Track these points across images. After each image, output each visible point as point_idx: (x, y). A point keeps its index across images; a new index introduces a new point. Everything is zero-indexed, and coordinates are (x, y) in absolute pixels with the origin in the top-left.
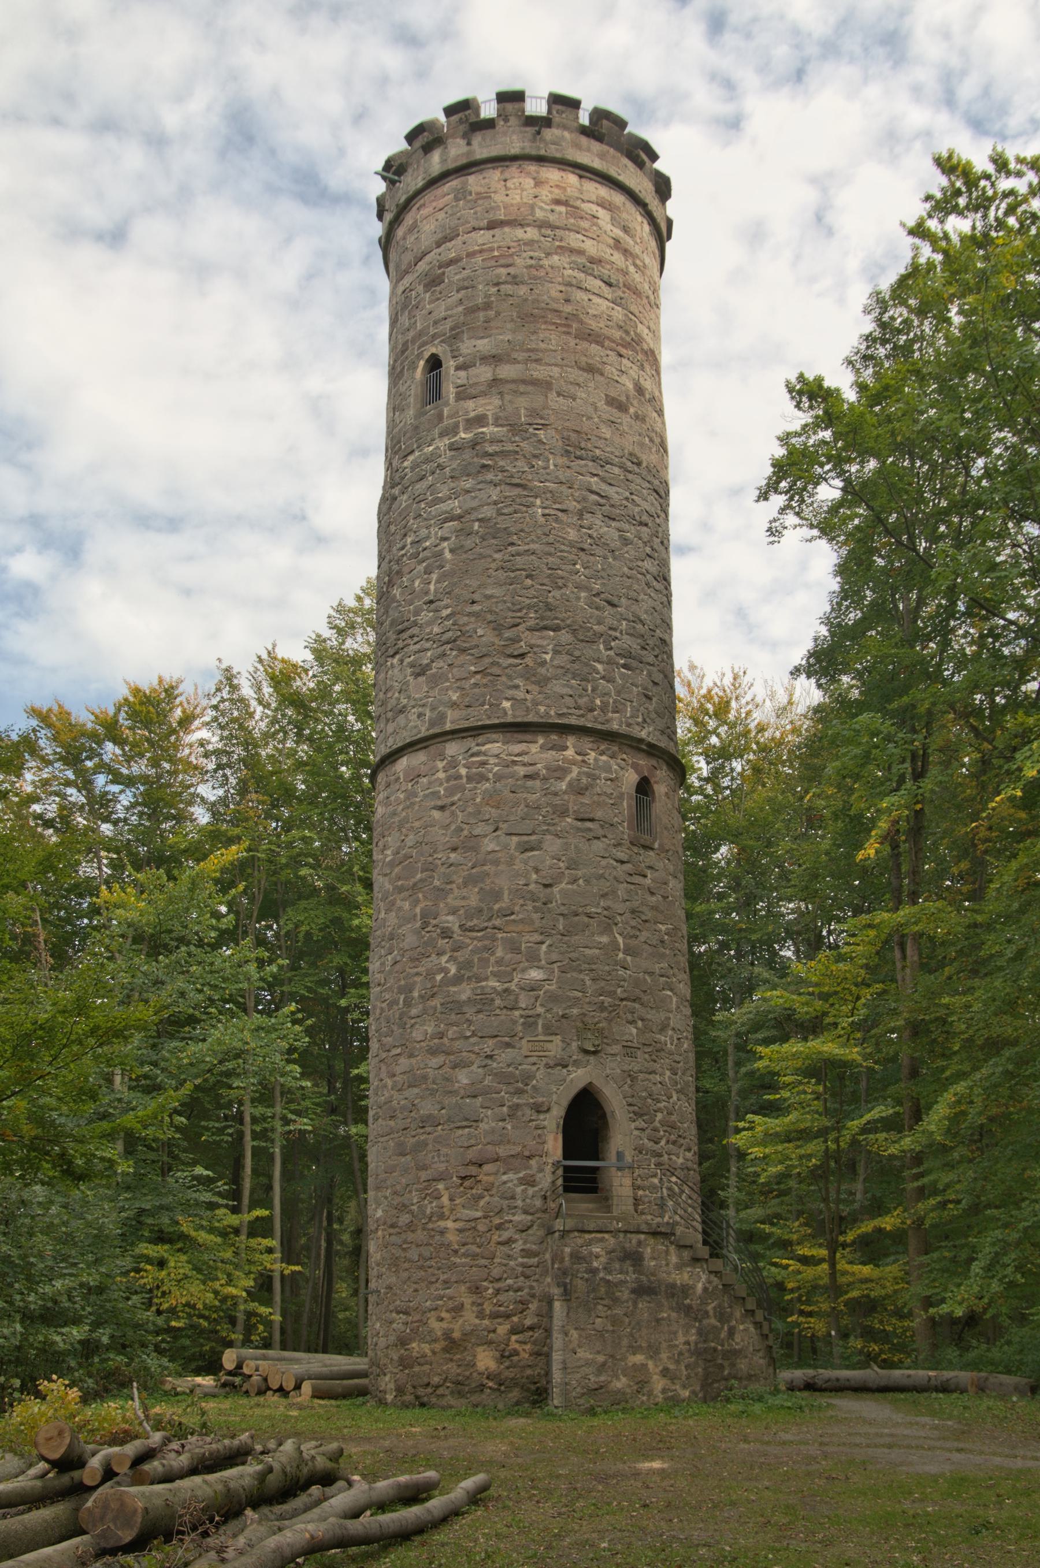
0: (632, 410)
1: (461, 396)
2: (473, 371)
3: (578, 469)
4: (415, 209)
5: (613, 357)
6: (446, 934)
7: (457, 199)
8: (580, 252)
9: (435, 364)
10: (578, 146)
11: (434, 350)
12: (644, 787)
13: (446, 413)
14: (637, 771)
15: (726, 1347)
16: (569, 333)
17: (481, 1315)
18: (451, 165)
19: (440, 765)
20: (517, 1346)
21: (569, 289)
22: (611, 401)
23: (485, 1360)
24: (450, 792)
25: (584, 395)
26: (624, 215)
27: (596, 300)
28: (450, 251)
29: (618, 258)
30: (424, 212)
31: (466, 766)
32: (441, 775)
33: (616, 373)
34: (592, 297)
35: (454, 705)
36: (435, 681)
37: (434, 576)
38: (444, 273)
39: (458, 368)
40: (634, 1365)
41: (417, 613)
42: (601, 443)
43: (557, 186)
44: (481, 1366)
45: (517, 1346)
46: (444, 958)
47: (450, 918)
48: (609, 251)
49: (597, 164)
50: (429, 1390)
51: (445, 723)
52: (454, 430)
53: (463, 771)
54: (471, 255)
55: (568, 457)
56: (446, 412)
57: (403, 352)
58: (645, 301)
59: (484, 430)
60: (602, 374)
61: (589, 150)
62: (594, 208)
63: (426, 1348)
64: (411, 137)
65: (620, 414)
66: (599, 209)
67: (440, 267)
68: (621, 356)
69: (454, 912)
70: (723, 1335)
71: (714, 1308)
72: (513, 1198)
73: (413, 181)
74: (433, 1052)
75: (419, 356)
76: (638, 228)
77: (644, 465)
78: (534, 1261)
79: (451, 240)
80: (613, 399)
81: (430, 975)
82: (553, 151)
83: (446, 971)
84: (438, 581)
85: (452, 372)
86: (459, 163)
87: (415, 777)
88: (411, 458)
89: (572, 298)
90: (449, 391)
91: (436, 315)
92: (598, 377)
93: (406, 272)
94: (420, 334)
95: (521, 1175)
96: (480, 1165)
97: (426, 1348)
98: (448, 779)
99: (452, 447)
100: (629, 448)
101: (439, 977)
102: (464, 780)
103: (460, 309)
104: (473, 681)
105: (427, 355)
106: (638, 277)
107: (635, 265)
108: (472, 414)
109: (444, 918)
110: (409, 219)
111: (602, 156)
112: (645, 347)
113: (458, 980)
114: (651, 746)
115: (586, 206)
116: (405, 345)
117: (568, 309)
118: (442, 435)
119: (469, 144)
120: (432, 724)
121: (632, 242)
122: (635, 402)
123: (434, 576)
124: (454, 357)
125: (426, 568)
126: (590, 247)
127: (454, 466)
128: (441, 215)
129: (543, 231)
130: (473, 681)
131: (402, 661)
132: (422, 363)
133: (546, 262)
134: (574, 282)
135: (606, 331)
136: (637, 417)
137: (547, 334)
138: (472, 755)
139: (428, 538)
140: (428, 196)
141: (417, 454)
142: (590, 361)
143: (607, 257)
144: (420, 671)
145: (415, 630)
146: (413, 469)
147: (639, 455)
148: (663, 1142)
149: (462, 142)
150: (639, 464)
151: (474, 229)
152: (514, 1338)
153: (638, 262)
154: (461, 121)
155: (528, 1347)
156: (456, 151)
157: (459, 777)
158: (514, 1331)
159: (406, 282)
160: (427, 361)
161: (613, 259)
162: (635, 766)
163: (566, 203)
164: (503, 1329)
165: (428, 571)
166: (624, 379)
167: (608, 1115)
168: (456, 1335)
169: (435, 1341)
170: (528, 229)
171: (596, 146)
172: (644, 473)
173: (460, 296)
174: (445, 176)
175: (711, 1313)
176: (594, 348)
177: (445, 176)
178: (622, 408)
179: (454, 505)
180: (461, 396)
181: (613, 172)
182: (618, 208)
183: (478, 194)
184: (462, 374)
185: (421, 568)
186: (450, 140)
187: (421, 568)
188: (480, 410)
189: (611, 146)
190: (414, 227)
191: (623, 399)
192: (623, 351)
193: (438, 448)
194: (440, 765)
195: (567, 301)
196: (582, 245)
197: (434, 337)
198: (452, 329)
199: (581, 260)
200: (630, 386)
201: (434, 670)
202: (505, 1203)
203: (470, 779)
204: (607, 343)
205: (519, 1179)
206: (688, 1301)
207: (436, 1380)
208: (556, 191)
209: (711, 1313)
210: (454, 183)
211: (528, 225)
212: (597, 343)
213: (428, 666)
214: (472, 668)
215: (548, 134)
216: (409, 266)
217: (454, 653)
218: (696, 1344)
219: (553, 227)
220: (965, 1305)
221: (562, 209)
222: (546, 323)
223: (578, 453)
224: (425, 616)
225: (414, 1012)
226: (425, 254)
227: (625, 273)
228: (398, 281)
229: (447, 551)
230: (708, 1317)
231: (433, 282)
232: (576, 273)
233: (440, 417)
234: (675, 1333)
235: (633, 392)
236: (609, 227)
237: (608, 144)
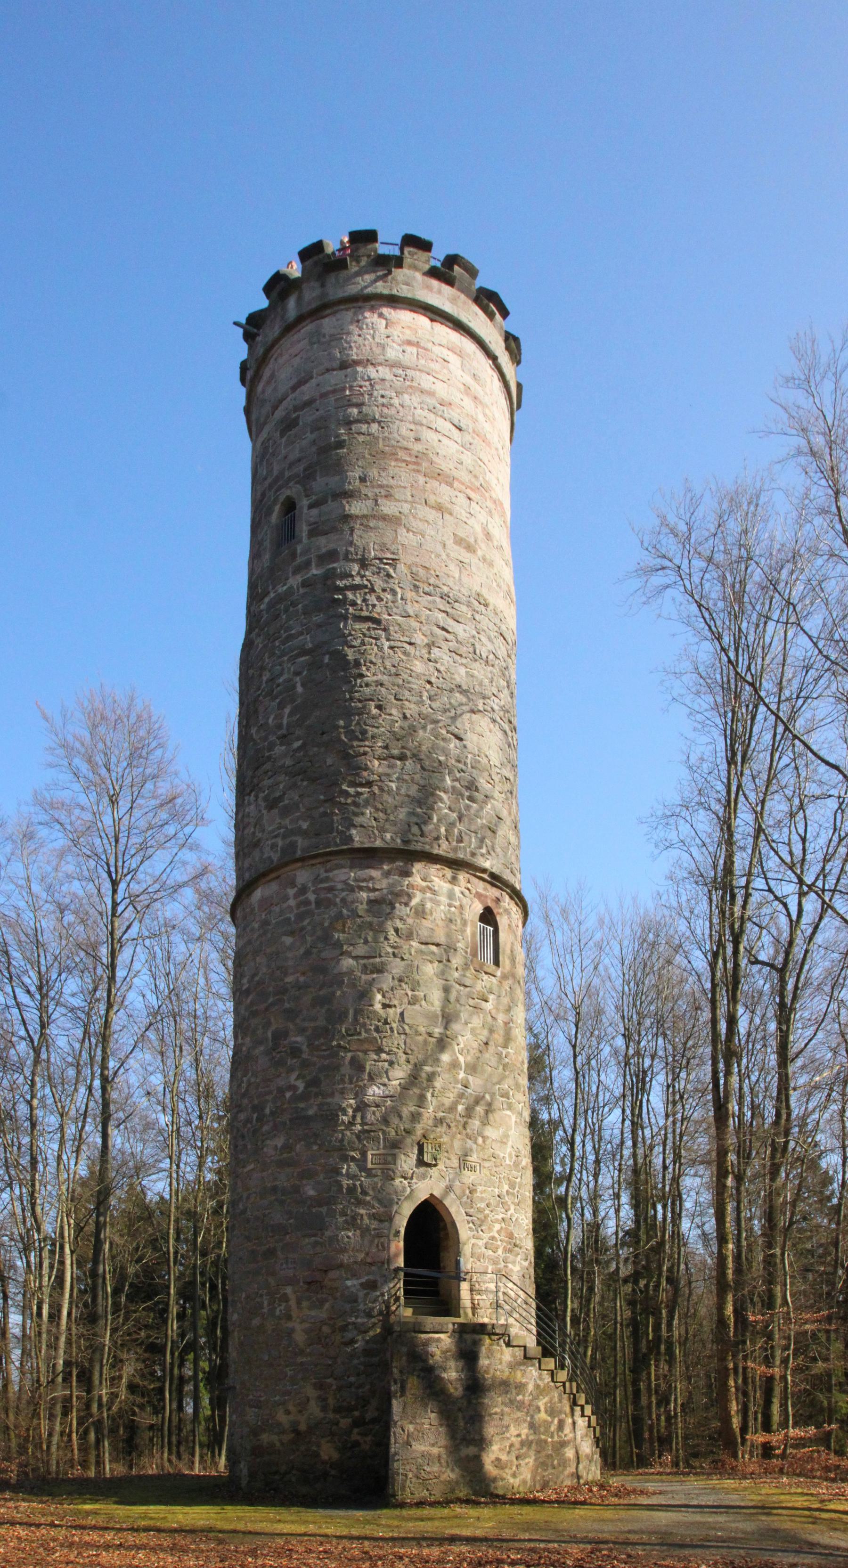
0: (480, 553)
1: (313, 533)
2: (324, 508)
3: (426, 604)
4: (272, 360)
5: (462, 500)
6: (295, 1052)
7: (312, 344)
8: (431, 394)
9: (290, 506)
10: (429, 288)
11: (288, 492)
12: (488, 917)
13: (299, 551)
14: (481, 902)
15: (556, 1438)
16: (418, 471)
17: (324, 1409)
18: (305, 309)
19: (291, 892)
20: (359, 1438)
21: (419, 427)
22: (459, 541)
23: (328, 1451)
24: (300, 917)
25: (433, 533)
26: (475, 364)
27: (445, 441)
28: (307, 391)
29: (467, 403)
30: (281, 361)
31: (314, 892)
32: (292, 902)
33: (464, 514)
34: (441, 438)
35: (305, 834)
36: (286, 812)
37: (287, 711)
38: (298, 417)
39: (310, 507)
40: (467, 1456)
41: (271, 747)
42: (450, 582)
43: (409, 327)
44: (324, 1456)
45: (359, 1438)
46: (294, 1076)
47: (299, 1039)
48: (459, 396)
49: (448, 308)
50: (277, 1477)
51: (295, 853)
52: (307, 564)
53: (312, 897)
54: (323, 396)
55: (417, 592)
56: (299, 549)
57: (261, 501)
58: (493, 451)
59: (335, 565)
60: (451, 514)
61: (439, 292)
62: (446, 353)
63: (275, 1438)
64: (268, 289)
65: (468, 555)
66: (450, 353)
67: (295, 411)
68: (470, 499)
69: (303, 1030)
70: (553, 1428)
71: (546, 1404)
72: (356, 1301)
73: (272, 331)
74: (282, 1164)
75: (275, 502)
76: (489, 380)
77: (491, 607)
78: (375, 1360)
79: (305, 382)
80: (462, 539)
81: (281, 1091)
82: (404, 291)
83: (293, 1088)
84: (290, 715)
85: (305, 510)
86: (314, 305)
87: (266, 903)
88: (266, 600)
89: (423, 438)
90: (303, 530)
91: (291, 458)
92: (447, 516)
93: (265, 423)
94: (277, 479)
95: (363, 1280)
96: (326, 1271)
97: (275, 1438)
98: (298, 906)
99: (305, 584)
100: (476, 588)
101: (288, 1095)
102: (313, 906)
103: (314, 449)
104: (322, 810)
105: (282, 498)
106: (487, 427)
107: (485, 415)
108: (324, 550)
109: (293, 1039)
110: (267, 373)
111: (453, 301)
112: (494, 496)
113: (305, 1097)
114: (493, 876)
115: (436, 349)
116: (263, 495)
117: (417, 447)
118: (295, 573)
119: (323, 285)
120: (284, 851)
121: (482, 393)
122: (483, 546)
123: (287, 711)
124: (307, 496)
125: (279, 703)
126: (441, 390)
127: (306, 602)
128: (297, 361)
129: (394, 370)
130: (322, 810)
131: (257, 797)
132: (277, 508)
133: (396, 401)
134: (424, 421)
135: (455, 473)
136: (484, 560)
137: (397, 470)
138: (322, 881)
139: (281, 674)
140: (286, 342)
141: (272, 595)
142: (439, 500)
143: (457, 401)
144: (272, 805)
145: (267, 766)
146: (268, 610)
147: (486, 596)
148: (500, 1251)
149: (316, 285)
150: (486, 605)
151: (328, 370)
152: (356, 1431)
153: (487, 411)
154: (316, 263)
155: (368, 1439)
156: (311, 294)
157: (307, 903)
158: (356, 1423)
159: (264, 435)
160: (282, 504)
161: (463, 404)
162: (479, 896)
163: (417, 345)
164: (345, 1422)
165: (281, 706)
166: (472, 521)
167: (449, 1226)
168: (303, 1427)
169: (283, 1432)
170: (380, 368)
171: (446, 289)
172: (491, 615)
173: (313, 436)
174: (301, 319)
175: (542, 1408)
176: (444, 489)
177: (301, 319)
178: (470, 548)
179: (308, 641)
180: (313, 533)
181: (464, 318)
182: (469, 356)
183: (331, 336)
184: (315, 512)
185: (275, 704)
186: (304, 286)
187: (275, 704)
188: (332, 546)
189: (462, 292)
190: (272, 376)
191: (472, 540)
192: (472, 495)
193: (291, 587)
194: (291, 892)
195: (417, 440)
196: (433, 387)
197: (290, 479)
198: (305, 470)
199: (432, 402)
200: (478, 529)
201: (286, 802)
202: (348, 1307)
203: (318, 903)
204: (456, 484)
205: (362, 1284)
206: (520, 1397)
207: (283, 1468)
208: (408, 332)
209: (542, 1408)
210: (308, 328)
211: (381, 364)
212: (447, 483)
213: (280, 798)
214: (322, 797)
215: (398, 273)
216: (267, 417)
217: (305, 783)
218: (527, 1435)
219: (405, 368)
220: (702, 1190)
221: (414, 350)
222: (397, 460)
223: (427, 589)
224: (279, 750)
225: (266, 1128)
226: (281, 401)
227: (475, 421)
228: (257, 436)
229: (299, 686)
230: (539, 1411)
231: (288, 425)
232: (426, 413)
233: (294, 556)
234: (507, 1427)
235: (481, 536)
236: (460, 372)
237: (459, 290)
